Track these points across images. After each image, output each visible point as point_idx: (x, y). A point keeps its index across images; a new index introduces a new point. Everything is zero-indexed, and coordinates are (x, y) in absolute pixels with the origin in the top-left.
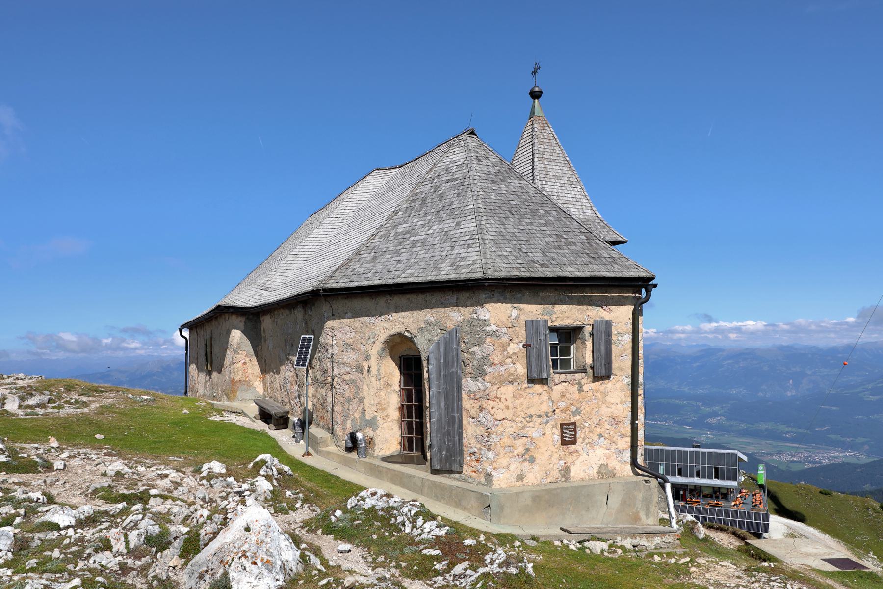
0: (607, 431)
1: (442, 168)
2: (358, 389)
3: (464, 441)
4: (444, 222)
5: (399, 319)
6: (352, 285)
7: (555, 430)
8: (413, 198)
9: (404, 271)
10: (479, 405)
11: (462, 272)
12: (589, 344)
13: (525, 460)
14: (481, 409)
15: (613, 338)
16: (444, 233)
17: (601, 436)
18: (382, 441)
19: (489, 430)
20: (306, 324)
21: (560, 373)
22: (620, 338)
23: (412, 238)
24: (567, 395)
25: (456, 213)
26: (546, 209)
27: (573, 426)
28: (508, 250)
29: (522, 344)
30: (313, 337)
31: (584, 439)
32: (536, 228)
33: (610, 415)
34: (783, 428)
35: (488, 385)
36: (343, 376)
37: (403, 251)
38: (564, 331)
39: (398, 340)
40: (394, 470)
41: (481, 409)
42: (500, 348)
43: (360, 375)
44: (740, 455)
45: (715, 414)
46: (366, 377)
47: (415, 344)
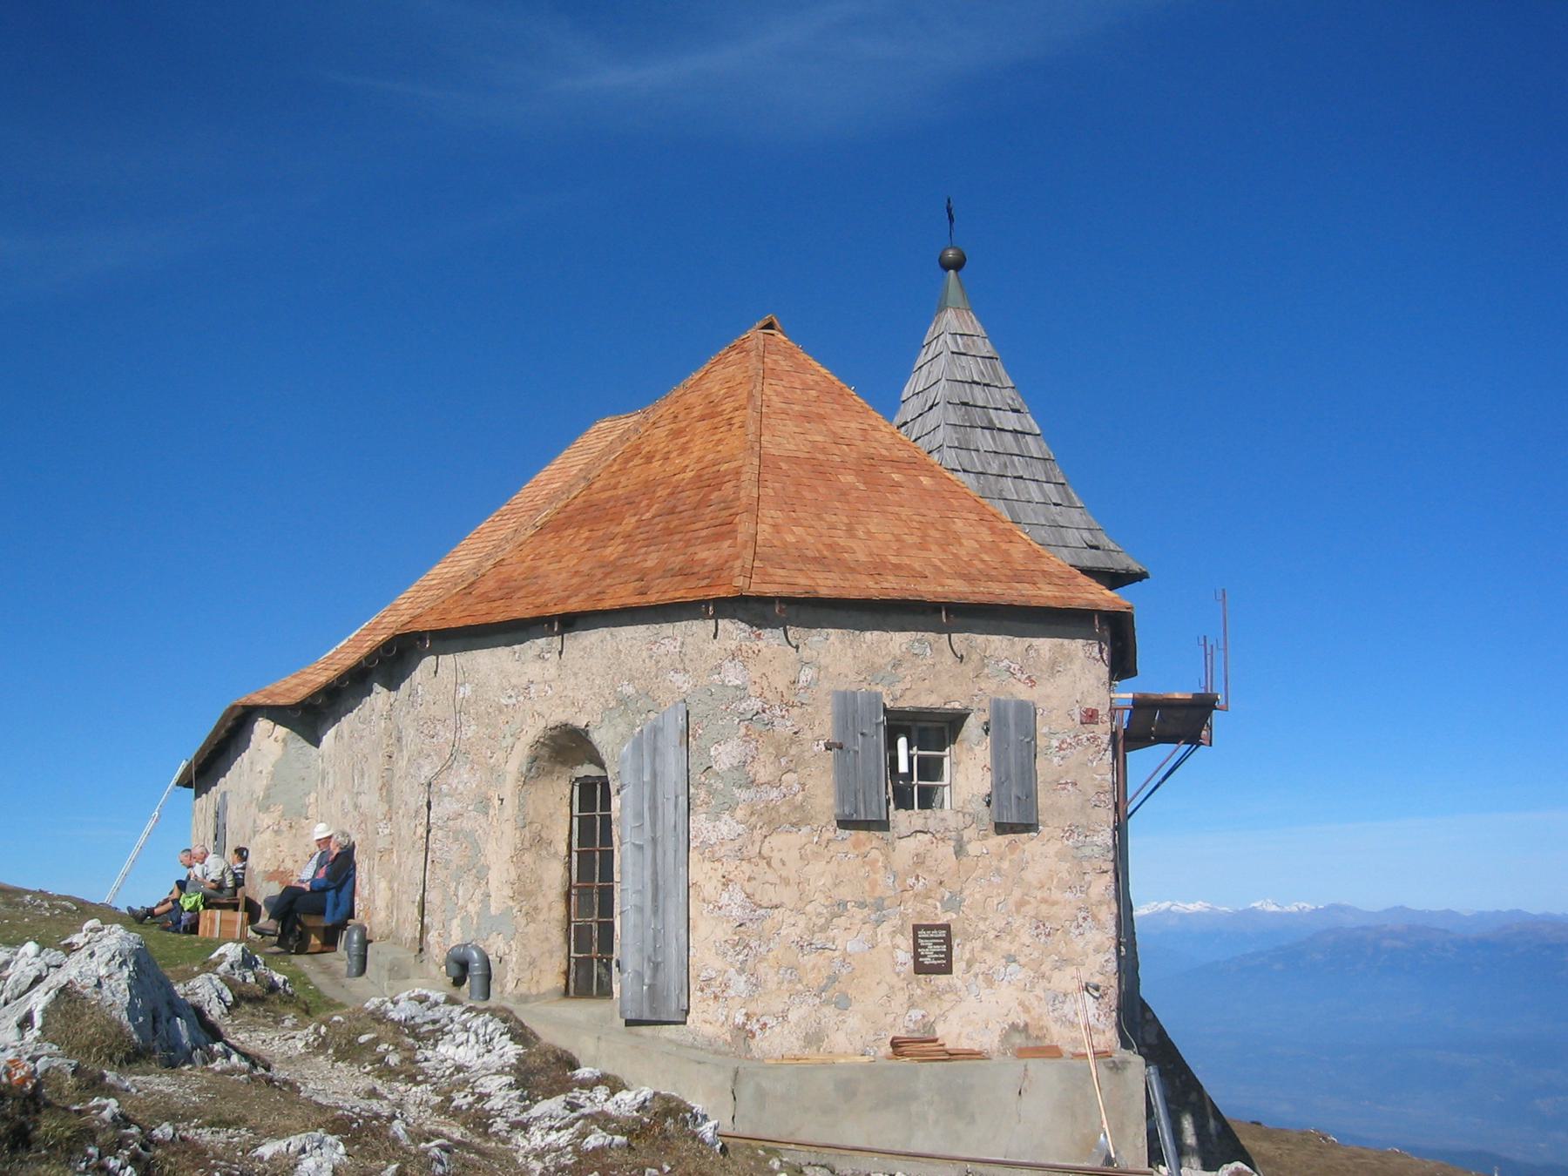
5: (565, 693)
7: (899, 940)
13: (826, 1003)
17: (1011, 959)
24: (930, 862)
27: (943, 933)
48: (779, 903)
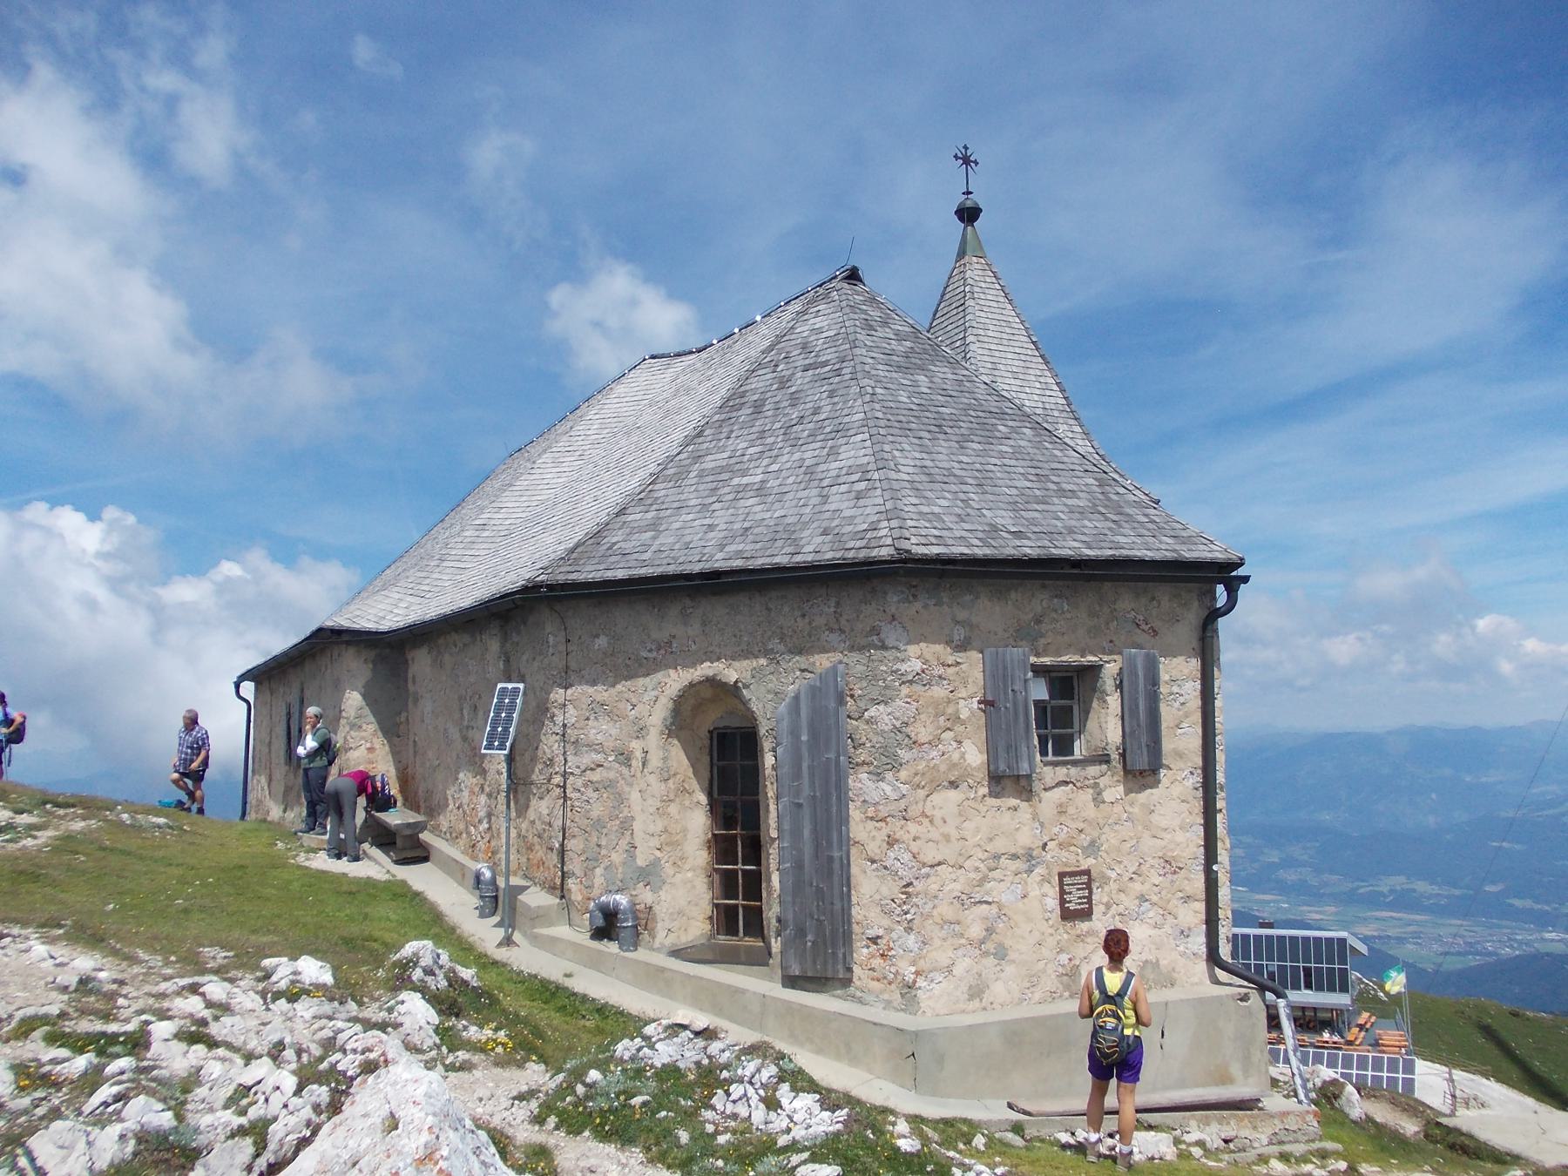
0: (1155, 888)
1: (793, 343)
2: (621, 799)
3: (854, 912)
4: (803, 448)
5: (710, 649)
6: (609, 575)
7: (1047, 888)
8: (732, 403)
9: (722, 547)
10: (885, 831)
11: (847, 546)
12: (1114, 701)
13: (986, 954)
14: (891, 842)
15: (1161, 690)
16: (803, 469)
17: (1143, 898)
18: (671, 914)
19: (910, 889)
20: (507, 661)
21: (1055, 764)
22: (1175, 689)
23: (736, 481)
24: (1071, 810)
25: (828, 429)
26: (1010, 423)
27: (1085, 879)
28: (944, 503)
29: (975, 700)
30: (521, 686)
31: (1108, 906)
32: (994, 461)
33: (1160, 854)
34: (1422, 886)
35: (904, 789)
36: (588, 772)
37: (717, 506)
38: (1060, 674)
39: (707, 693)
40: (701, 978)
41: (891, 842)
42: (930, 710)
43: (625, 770)
44: (1353, 942)
45: (1289, 863)
46: (639, 774)
47: (745, 703)
48: (869, 821)
